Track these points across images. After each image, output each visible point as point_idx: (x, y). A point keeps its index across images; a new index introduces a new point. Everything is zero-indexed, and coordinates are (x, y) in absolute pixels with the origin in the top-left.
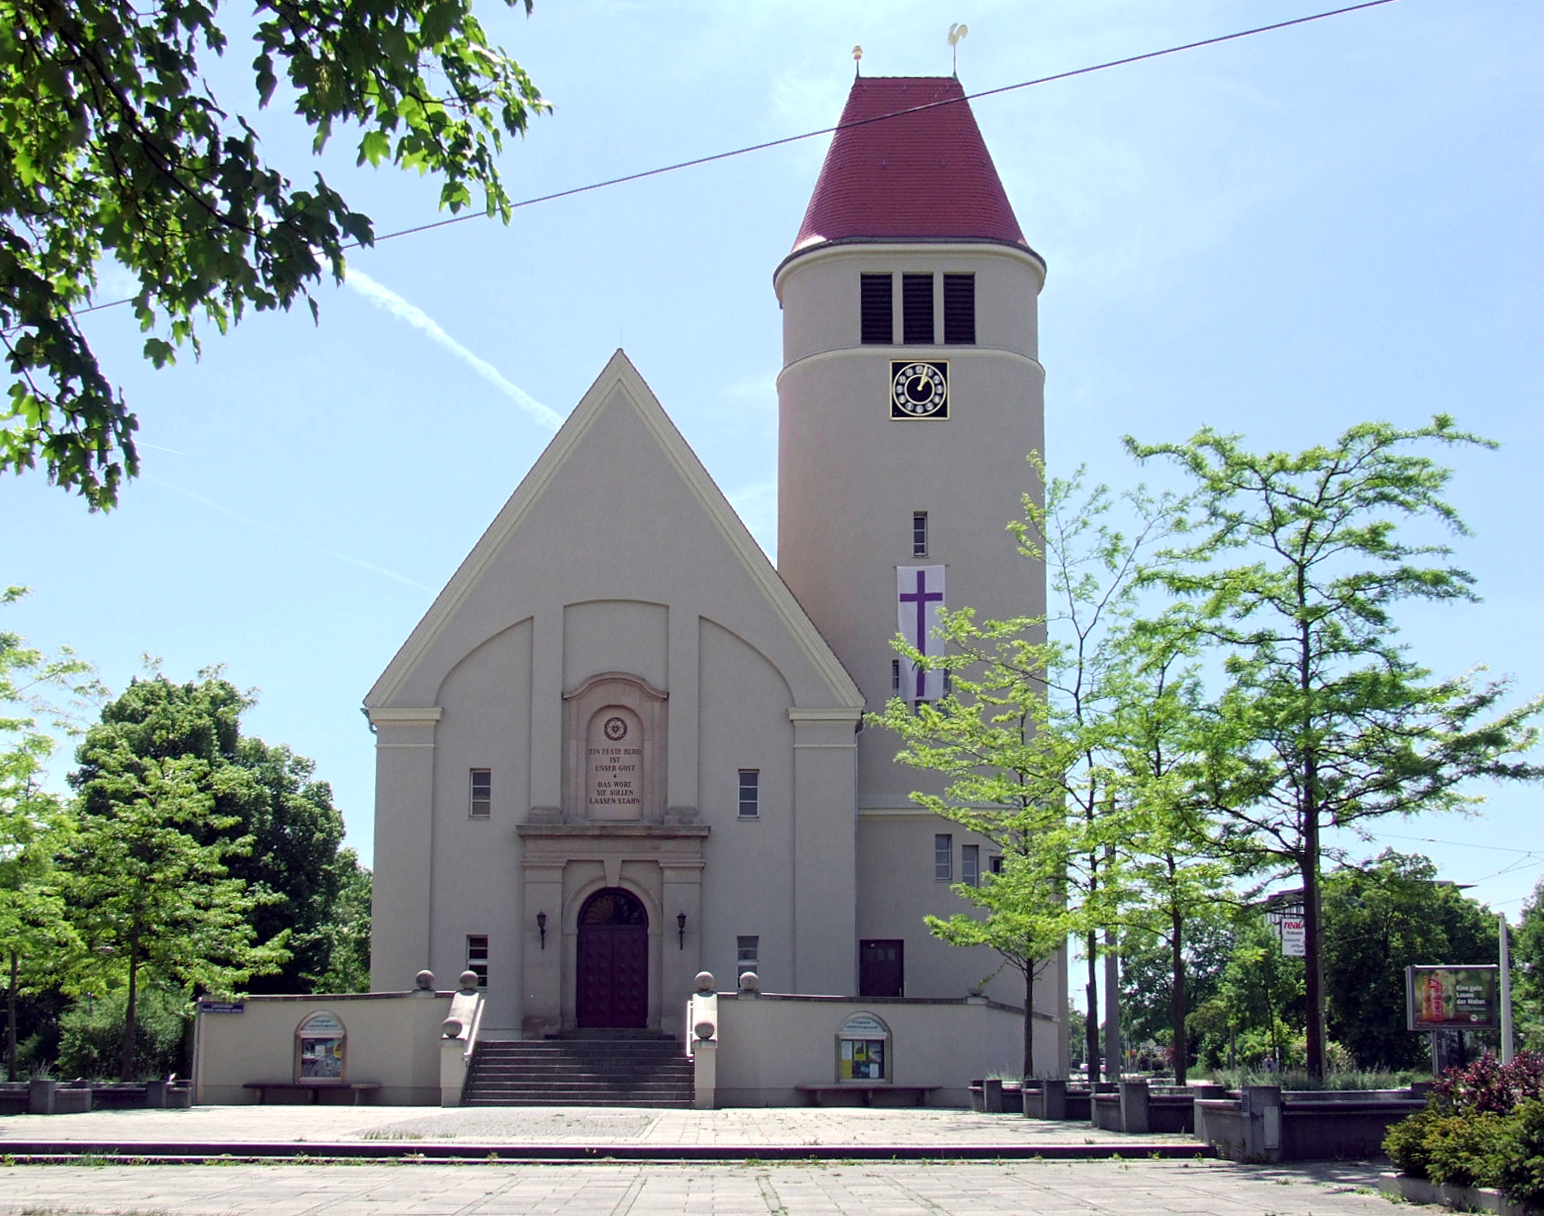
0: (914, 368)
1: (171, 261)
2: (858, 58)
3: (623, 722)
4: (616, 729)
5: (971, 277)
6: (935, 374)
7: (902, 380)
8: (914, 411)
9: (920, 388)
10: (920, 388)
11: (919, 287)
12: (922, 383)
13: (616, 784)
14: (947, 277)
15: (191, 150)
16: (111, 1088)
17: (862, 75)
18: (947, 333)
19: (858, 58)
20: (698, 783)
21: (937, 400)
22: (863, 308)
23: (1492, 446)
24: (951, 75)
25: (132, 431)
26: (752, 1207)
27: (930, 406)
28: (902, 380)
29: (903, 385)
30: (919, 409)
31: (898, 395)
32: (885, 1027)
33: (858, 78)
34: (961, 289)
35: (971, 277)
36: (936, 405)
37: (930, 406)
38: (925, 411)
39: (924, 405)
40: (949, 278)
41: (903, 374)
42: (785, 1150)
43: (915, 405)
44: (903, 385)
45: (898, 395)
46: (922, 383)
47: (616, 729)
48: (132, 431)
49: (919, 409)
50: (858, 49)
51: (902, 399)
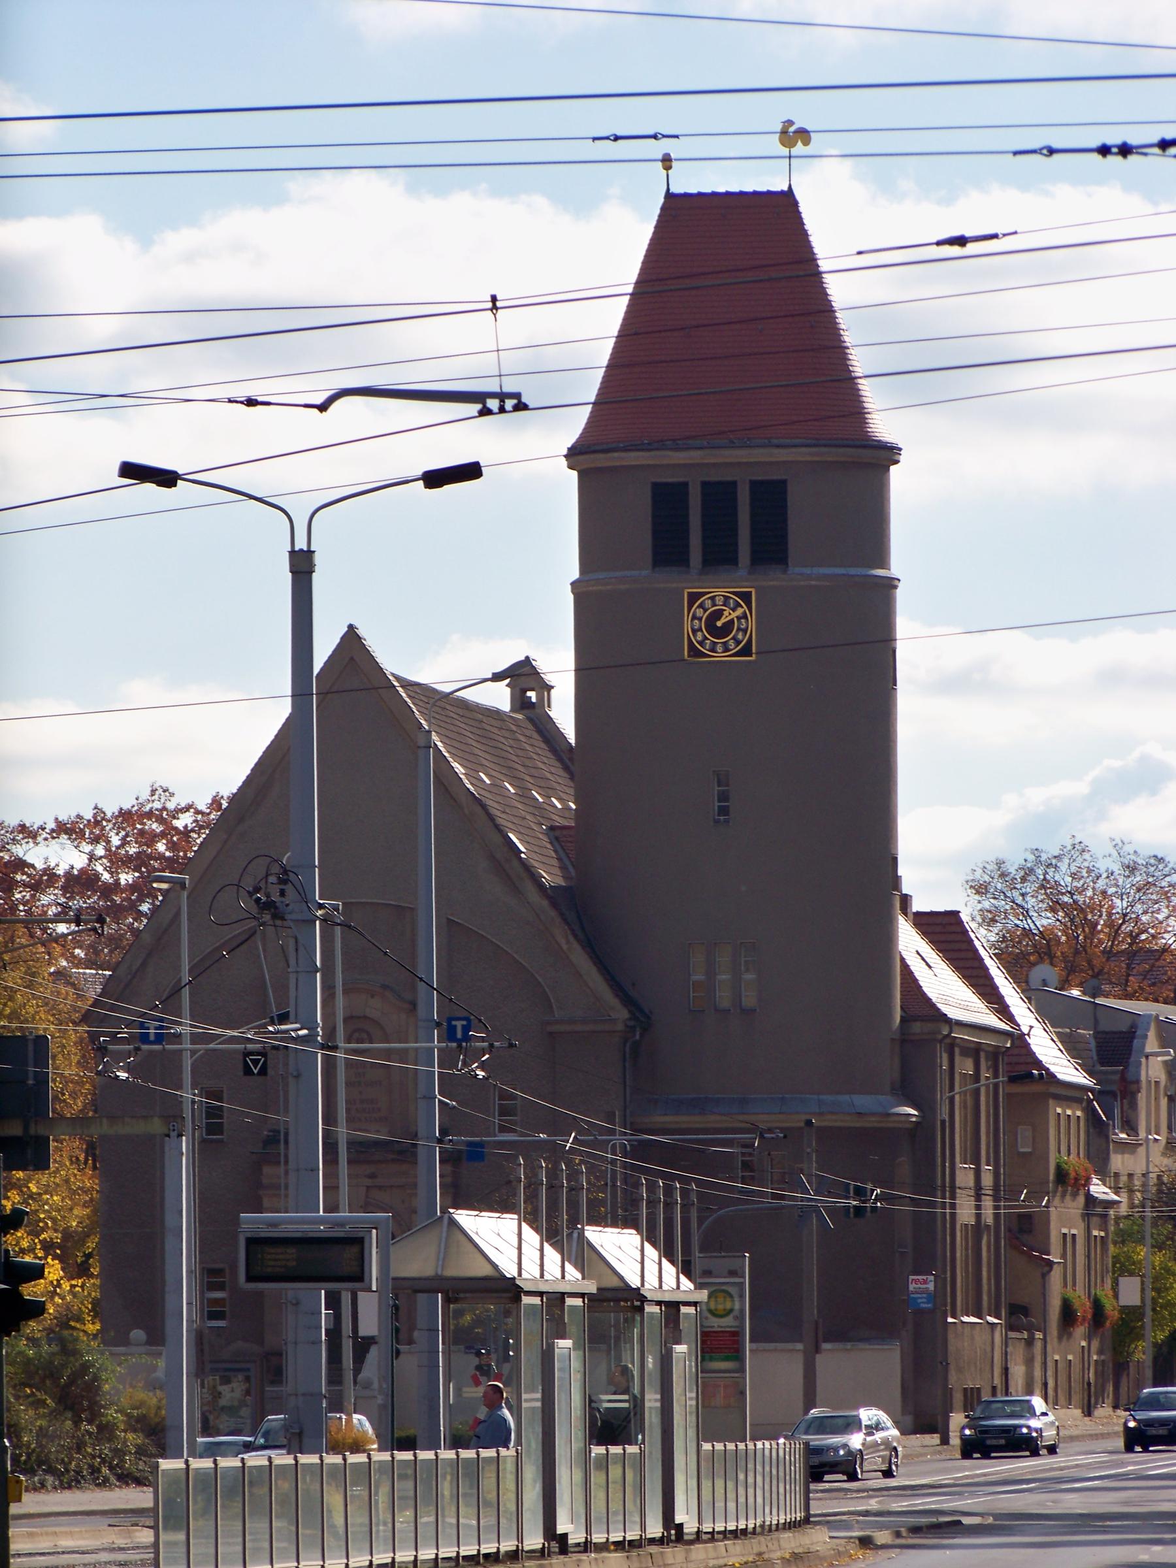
1: (117, 882)
5: (784, 482)
8: (713, 650)
9: (719, 624)
10: (719, 624)
11: (719, 496)
12: (723, 620)
14: (705, 484)
15: (8, 1198)
17: (675, 189)
18: (705, 553)
20: (52, 865)
21: (740, 636)
24: (786, 188)
25: (799, 143)
26: (290, 1357)
28: (700, 612)
29: (700, 619)
30: (719, 648)
31: (694, 632)
33: (669, 196)
34: (771, 497)
35: (784, 482)
36: (738, 642)
40: (756, 487)
44: (700, 619)
45: (694, 632)
46: (723, 620)
48: (799, 143)
49: (719, 648)
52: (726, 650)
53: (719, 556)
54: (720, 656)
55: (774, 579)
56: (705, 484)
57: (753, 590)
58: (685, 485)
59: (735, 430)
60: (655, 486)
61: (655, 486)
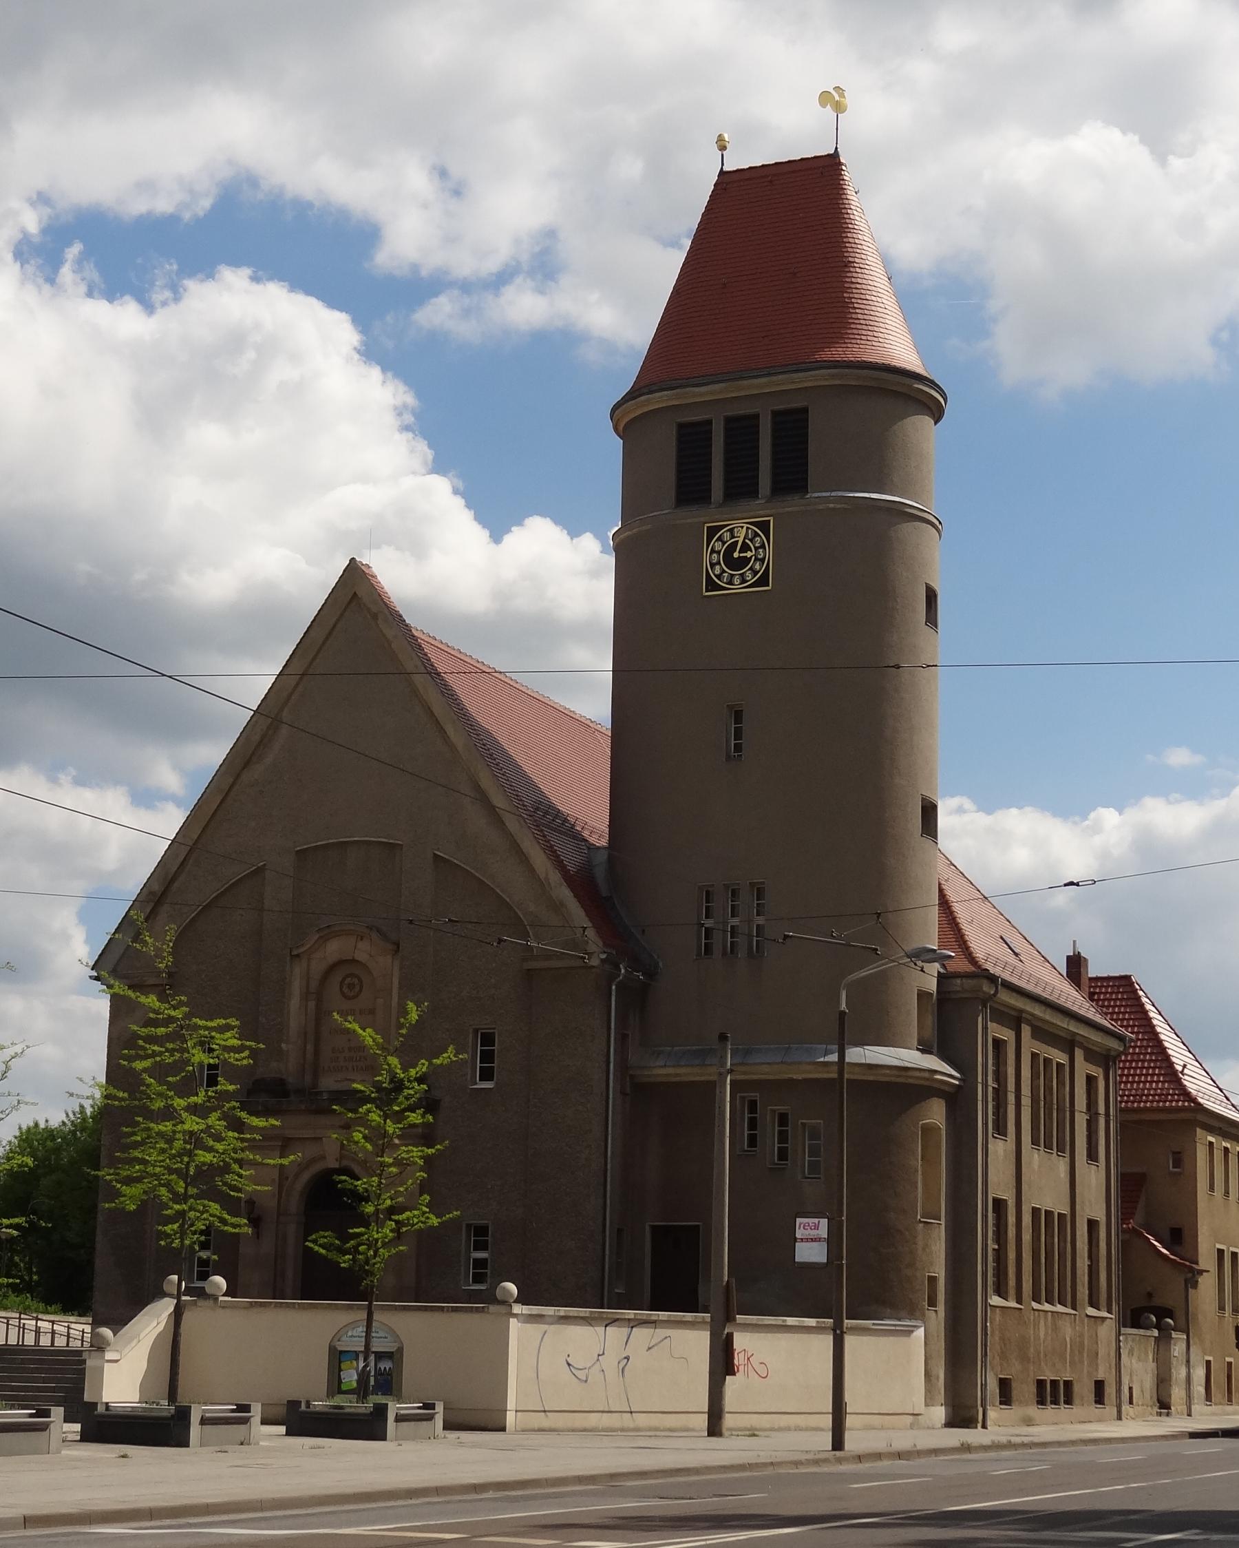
0: (731, 531)
2: (723, 148)
3: (347, 976)
4: (351, 986)
6: (757, 535)
7: (718, 546)
8: (730, 583)
13: (350, 1049)
14: (775, 414)
16: (326, 1410)
19: (723, 148)
21: (757, 567)
22: (679, 464)
23: (738, 716)
27: (749, 575)
28: (718, 546)
29: (719, 552)
30: (737, 580)
31: (713, 565)
32: (397, 1338)
33: (722, 173)
37: (749, 575)
38: (744, 581)
39: (742, 575)
41: (719, 539)
42: (719, 1516)
43: (732, 576)
47: (351, 986)
49: (737, 580)
50: (720, 139)
51: (717, 570)
52: (744, 581)
53: (741, 488)
54: (737, 588)
55: (792, 505)
56: (775, 414)
57: (771, 519)
58: (756, 417)
59: (765, 388)
60: (681, 426)
61: (681, 426)
